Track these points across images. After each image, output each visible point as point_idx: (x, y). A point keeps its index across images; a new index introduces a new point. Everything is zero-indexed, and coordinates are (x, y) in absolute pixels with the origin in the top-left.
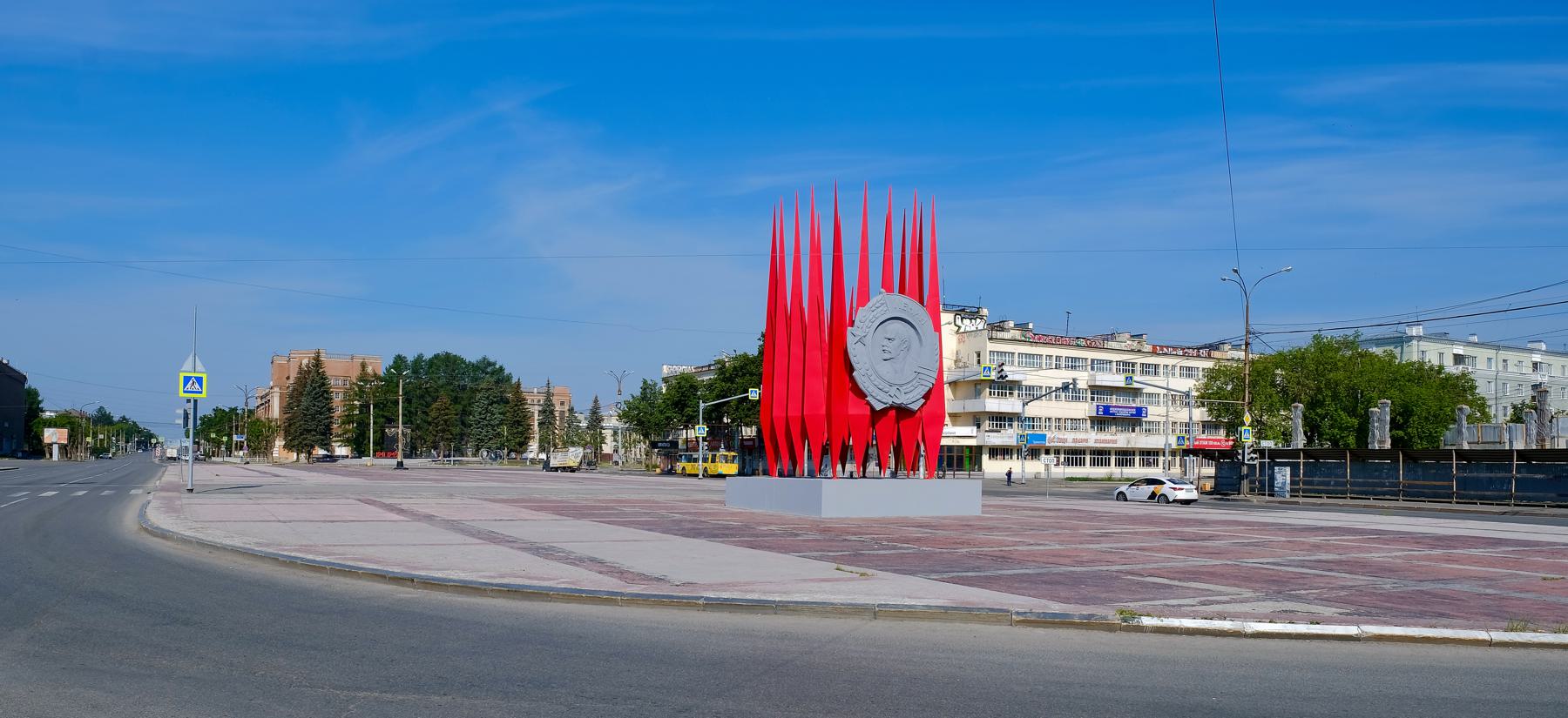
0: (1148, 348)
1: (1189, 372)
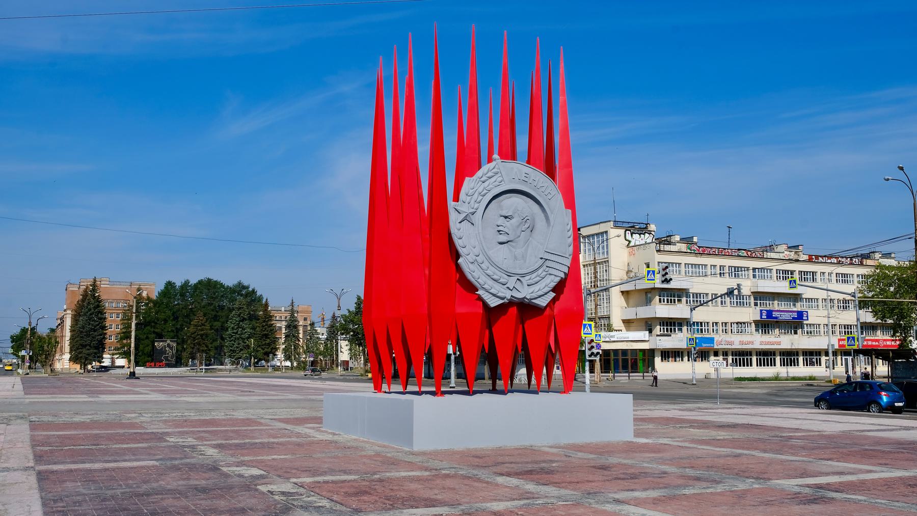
0: (806, 257)
1: (844, 278)
